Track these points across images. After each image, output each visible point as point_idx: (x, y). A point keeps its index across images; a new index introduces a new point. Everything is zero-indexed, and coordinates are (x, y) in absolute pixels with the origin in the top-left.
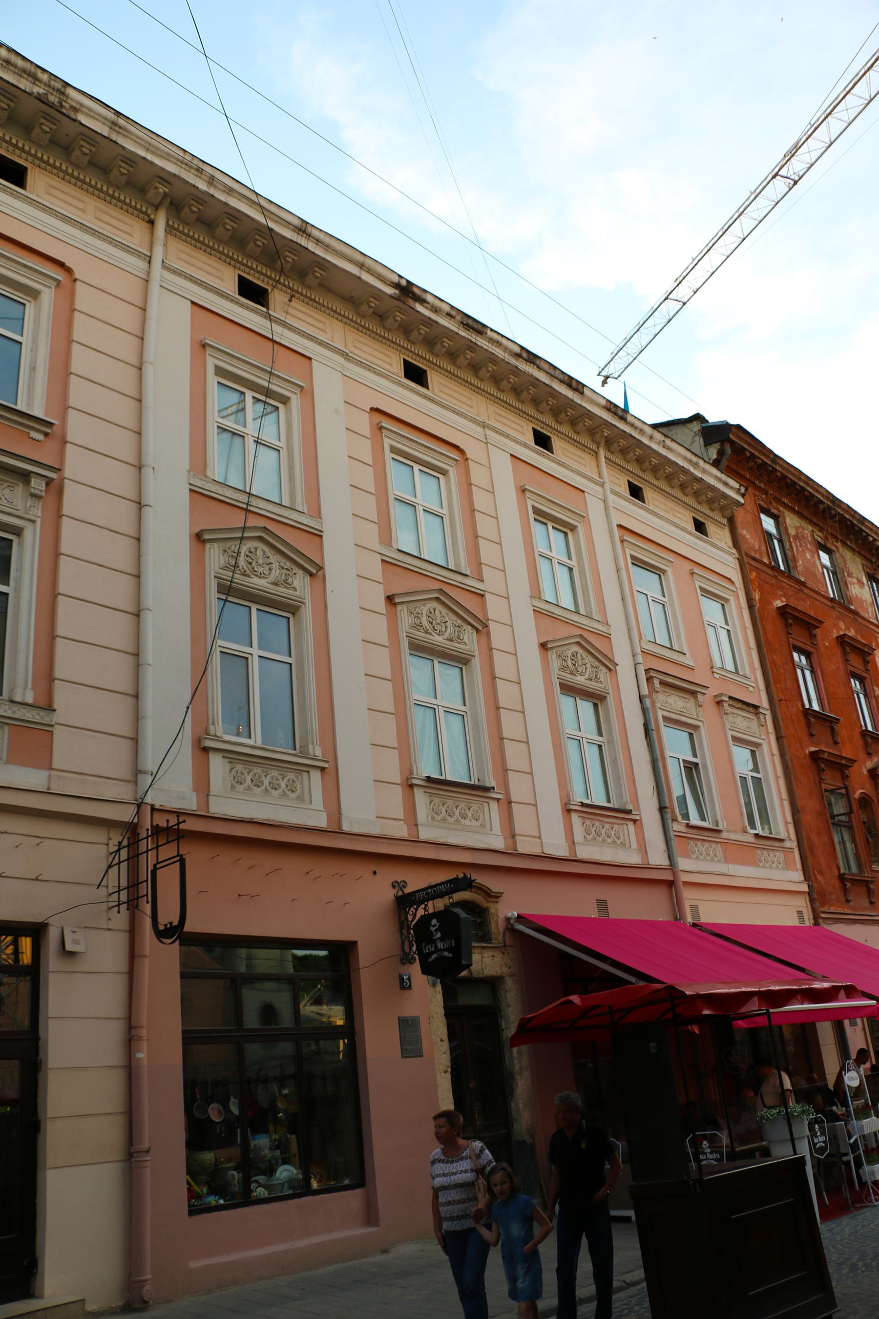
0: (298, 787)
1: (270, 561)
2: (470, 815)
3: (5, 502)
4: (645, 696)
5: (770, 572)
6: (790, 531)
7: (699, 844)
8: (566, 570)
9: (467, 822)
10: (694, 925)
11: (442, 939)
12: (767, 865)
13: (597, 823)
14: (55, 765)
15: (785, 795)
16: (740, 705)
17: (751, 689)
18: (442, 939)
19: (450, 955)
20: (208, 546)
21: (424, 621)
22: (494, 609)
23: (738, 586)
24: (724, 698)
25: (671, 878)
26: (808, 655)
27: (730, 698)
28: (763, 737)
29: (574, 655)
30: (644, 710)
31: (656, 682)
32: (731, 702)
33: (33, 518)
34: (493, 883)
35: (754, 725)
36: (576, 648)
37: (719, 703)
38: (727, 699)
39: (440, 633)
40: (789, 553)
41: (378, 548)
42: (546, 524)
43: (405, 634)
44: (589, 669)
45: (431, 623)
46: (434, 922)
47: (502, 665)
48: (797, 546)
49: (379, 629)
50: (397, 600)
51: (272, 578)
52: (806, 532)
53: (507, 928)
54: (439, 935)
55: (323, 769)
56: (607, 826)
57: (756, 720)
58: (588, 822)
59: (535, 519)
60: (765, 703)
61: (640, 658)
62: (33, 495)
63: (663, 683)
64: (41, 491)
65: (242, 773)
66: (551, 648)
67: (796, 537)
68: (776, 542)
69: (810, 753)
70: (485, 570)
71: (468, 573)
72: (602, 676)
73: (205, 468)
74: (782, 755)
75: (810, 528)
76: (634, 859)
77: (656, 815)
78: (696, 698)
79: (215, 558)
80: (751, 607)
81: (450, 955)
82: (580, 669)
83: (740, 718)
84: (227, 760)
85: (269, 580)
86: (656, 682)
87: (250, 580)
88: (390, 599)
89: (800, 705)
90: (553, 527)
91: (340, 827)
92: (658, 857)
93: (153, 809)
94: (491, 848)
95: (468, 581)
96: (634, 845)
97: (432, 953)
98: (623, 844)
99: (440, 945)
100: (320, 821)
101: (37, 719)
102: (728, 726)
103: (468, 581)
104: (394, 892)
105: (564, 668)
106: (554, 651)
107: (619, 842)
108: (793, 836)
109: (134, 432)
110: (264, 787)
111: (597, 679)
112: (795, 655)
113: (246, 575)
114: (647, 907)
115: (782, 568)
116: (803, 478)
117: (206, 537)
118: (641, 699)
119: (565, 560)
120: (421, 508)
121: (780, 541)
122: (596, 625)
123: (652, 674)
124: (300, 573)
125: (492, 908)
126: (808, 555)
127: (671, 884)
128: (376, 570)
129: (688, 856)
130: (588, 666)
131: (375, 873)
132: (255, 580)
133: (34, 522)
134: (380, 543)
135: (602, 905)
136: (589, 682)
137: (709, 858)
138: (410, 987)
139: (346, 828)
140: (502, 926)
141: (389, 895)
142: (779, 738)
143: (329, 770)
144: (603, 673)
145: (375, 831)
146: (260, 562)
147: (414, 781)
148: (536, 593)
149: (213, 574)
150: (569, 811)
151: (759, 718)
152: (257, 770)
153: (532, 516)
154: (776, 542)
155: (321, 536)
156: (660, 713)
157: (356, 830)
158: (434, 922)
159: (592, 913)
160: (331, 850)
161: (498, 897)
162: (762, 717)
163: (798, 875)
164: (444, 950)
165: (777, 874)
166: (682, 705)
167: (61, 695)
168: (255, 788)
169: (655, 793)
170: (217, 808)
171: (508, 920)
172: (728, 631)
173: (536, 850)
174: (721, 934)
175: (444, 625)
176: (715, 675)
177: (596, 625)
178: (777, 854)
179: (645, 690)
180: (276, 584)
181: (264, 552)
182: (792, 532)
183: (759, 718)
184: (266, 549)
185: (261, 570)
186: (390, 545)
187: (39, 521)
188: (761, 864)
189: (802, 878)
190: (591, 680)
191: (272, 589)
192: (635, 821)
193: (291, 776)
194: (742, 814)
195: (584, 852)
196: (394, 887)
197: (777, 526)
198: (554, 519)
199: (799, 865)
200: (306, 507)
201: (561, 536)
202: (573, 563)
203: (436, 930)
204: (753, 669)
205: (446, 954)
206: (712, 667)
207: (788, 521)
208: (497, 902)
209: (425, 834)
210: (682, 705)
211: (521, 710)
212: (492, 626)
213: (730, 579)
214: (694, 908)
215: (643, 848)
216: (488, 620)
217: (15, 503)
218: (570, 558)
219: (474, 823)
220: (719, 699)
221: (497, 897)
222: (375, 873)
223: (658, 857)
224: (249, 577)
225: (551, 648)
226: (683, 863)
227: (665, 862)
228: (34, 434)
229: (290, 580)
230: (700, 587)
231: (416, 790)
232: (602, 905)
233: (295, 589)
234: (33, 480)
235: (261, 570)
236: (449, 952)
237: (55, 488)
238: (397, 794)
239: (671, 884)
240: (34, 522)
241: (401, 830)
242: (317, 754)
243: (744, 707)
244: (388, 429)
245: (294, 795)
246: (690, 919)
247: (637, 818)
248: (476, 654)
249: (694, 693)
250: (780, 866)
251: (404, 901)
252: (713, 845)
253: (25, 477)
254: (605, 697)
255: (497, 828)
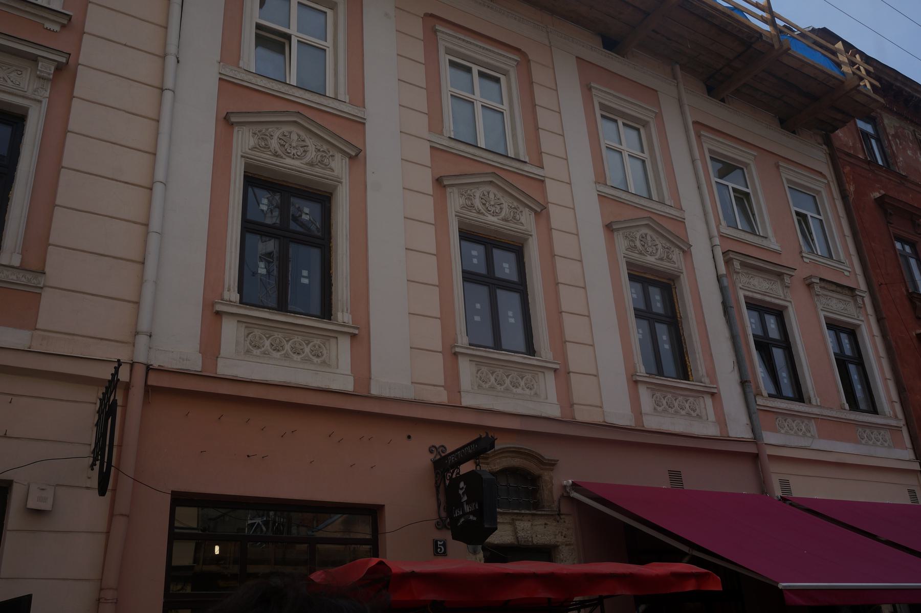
0: (325, 352)
1: (304, 144)
2: (522, 383)
3: (10, 84)
4: (723, 275)
5: (865, 166)
6: (888, 130)
7: (789, 420)
8: (639, 163)
9: (519, 390)
10: (783, 499)
11: (468, 502)
12: (871, 443)
13: (669, 396)
14: (38, 326)
15: (888, 374)
16: (834, 288)
17: (847, 273)
18: (468, 502)
19: (475, 519)
20: (449, 190)
21: (477, 203)
22: (554, 192)
23: (830, 179)
24: (814, 280)
25: (754, 451)
26: (913, 245)
27: (821, 279)
28: (861, 318)
29: (644, 237)
30: (722, 289)
31: (737, 265)
32: (823, 284)
33: (39, 98)
34: (547, 451)
35: (851, 309)
36: (644, 231)
37: (810, 286)
38: (818, 281)
39: (495, 214)
40: (888, 151)
41: (426, 135)
42: (616, 121)
43: (454, 213)
44: (660, 250)
45: (484, 204)
46: (462, 485)
47: (561, 243)
48: (896, 144)
49: (426, 208)
50: (446, 183)
51: (308, 159)
52: (906, 131)
53: (562, 496)
54: (465, 498)
55: (555, 370)
56: (680, 398)
57: (852, 303)
58: (658, 394)
59: (603, 116)
60: (863, 286)
61: (717, 241)
62: (39, 77)
63: (743, 264)
64: (49, 74)
65: (260, 338)
66: (618, 230)
67: (896, 136)
68: (873, 142)
69: (918, 335)
70: (546, 159)
71: (527, 160)
72: (674, 257)
73: (239, 59)
74: (884, 336)
75: (912, 128)
76: (712, 430)
77: (737, 390)
78: (782, 280)
79: (244, 141)
80: (844, 197)
81: (475, 519)
82: (650, 250)
83: (835, 301)
84: (244, 325)
85: (304, 161)
86: (737, 265)
87: (282, 161)
88: (439, 182)
89: (904, 290)
90: (624, 124)
91: (369, 390)
92: (739, 428)
93: (149, 368)
94: (543, 415)
95: (527, 168)
96: (712, 417)
97: (460, 517)
98: (699, 417)
99: (467, 508)
100: (348, 385)
101: (24, 281)
102: (820, 307)
103: (527, 168)
104: (432, 456)
105: (632, 248)
106: (621, 232)
107: (694, 414)
108: (900, 415)
109: (161, 26)
110: (283, 352)
111: (669, 260)
112: (898, 246)
113: (277, 156)
114: (733, 481)
115: (880, 163)
116: (899, 78)
117: (233, 119)
118: (719, 278)
119: (638, 153)
120: (480, 104)
121: (878, 141)
122: (668, 210)
123: (731, 255)
124: (338, 156)
125: (546, 476)
126: (909, 152)
127: (755, 457)
128: (425, 155)
129: (775, 430)
130: (659, 246)
131: (409, 437)
132: (288, 161)
133: (40, 102)
134: (430, 131)
135: (675, 476)
136: (659, 262)
137: (800, 434)
138: (445, 554)
139: (374, 391)
140: (556, 494)
141: (426, 460)
142: (879, 320)
143: (359, 337)
144: (676, 255)
145: (409, 395)
146: (294, 144)
147: (458, 350)
148: (600, 178)
149: (240, 153)
150: (636, 382)
151: (855, 301)
152: (278, 335)
153: (598, 112)
154: (873, 142)
155: (364, 124)
156: (741, 294)
157: (386, 394)
158: (462, 485)
159: (665, 483)
160: (358, 414)
161: (554, 465)
162: (859, 300)
163: (909, 454)
164: (470, 513)
165: (881, 452)
166: (767, 286)
167: (54, 258)
168: (274, 352)
169: (736, 368)
170: (225, 368)
171: (565, 487)
172: (821, 220)
173: (598, 419)
174: (813, 510)
175: (498, 207)
176: (805, 260)
177: (668, 210)
178: (882, 432)
179: (723, 270)
180: (311, 164)
181: (298, 135)
182: (891, 131)
183: (855, 301)
184: (301, 133)
185: (294, 151)
186: (441, 133)
187: (45, 102)
188: (863, 442)
189: (912, 456)
190: (662, 259)
191: (307, 169)
192: (713, 394)
193: (317, 342)
194: (838, 392)
195: (652, 422)
196: (431, 452)
197: (875, 128)
198: (623, 115)
199: (908, 443)
200: (347, 97)
201: (634, 134)
202: (646, 155)
203: (463, 493)
204: (848, 255)
205: (471, 517)
206: (801, 252)
207: (886, 121)
208: (552, 470)
209: (467, 401)
210: (767, 286)
211: (582, 285)
212: (552, 209)
213: (821, 173)
214: (785, 484)
215: (721, 420)
216: (548, 203)
217: (22, 86)
218: (643, 152)
219: (528, 391)
220: (809, 281)
221: (551, 465)
222: (409, 437)
223: (739, 428)
224: (282, 157)
225: (618, 230)
226: (769, 437)
227: (747, 434)
228: (48, 25)
229: (326, 161)
230: (787, 179)
231: (460, 359)
232: (675, 476)
233: (332, 170)
234: (40, 64)
235: (294, 151)
236: (474, 516)
237: (65, 71)
238: (437, 362)
239: (755, 457)
240: (40, 102)
241: (442, 397)
242: (346, 320)
243: (839, 289)
244: (443, 32)
245: (319, 360)
246: (778, 493)
247: (715, 391)
248: (534, 233)
249: (780, 275)
250: (886, 444)
251: (443, 465)
252: (806, 421)
253: (34, 59)
254: (679, 277)
255: (553, 396)
